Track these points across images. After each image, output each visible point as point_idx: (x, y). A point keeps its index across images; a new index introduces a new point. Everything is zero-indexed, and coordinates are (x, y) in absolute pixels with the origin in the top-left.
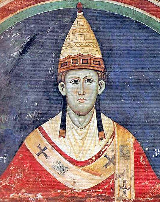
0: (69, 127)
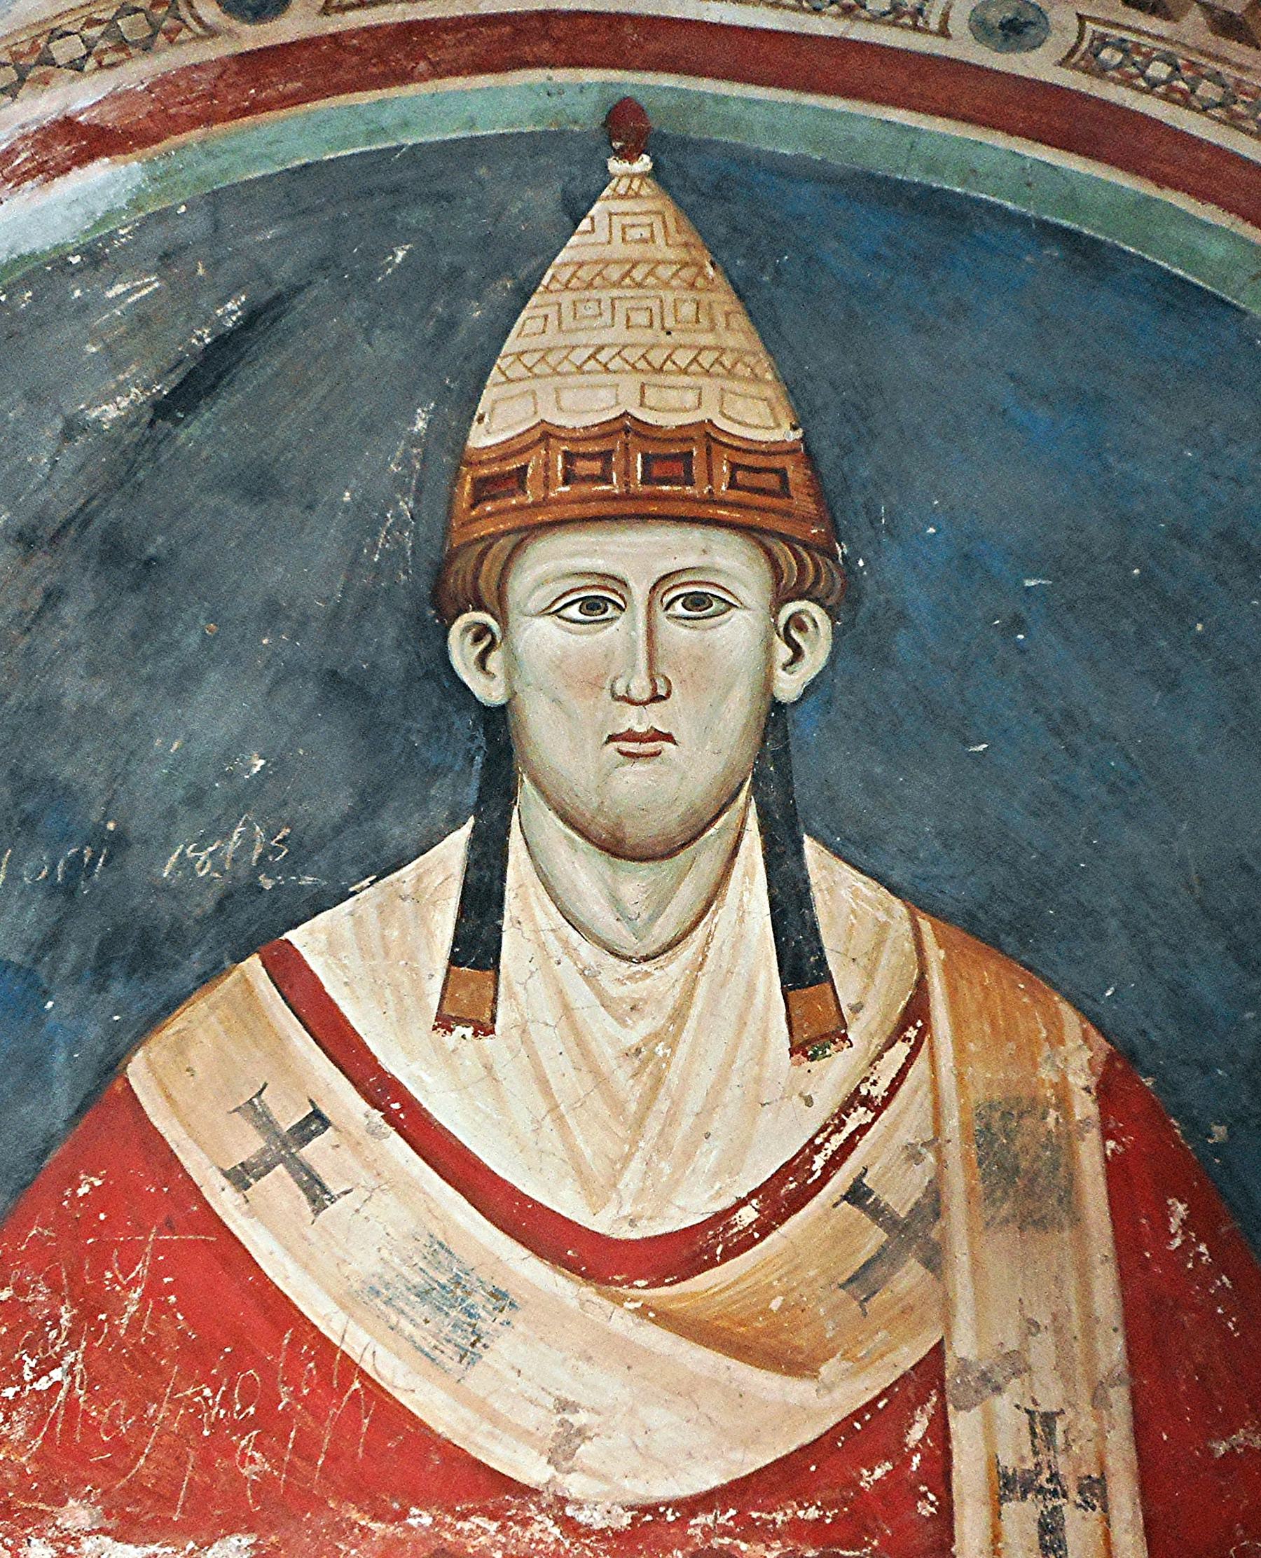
0: (530, 949)
